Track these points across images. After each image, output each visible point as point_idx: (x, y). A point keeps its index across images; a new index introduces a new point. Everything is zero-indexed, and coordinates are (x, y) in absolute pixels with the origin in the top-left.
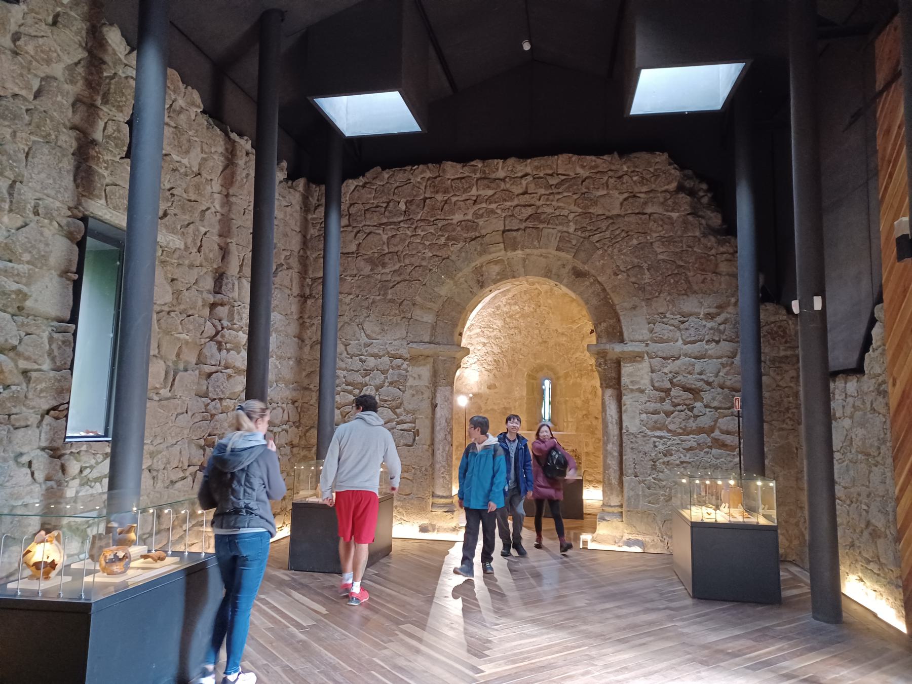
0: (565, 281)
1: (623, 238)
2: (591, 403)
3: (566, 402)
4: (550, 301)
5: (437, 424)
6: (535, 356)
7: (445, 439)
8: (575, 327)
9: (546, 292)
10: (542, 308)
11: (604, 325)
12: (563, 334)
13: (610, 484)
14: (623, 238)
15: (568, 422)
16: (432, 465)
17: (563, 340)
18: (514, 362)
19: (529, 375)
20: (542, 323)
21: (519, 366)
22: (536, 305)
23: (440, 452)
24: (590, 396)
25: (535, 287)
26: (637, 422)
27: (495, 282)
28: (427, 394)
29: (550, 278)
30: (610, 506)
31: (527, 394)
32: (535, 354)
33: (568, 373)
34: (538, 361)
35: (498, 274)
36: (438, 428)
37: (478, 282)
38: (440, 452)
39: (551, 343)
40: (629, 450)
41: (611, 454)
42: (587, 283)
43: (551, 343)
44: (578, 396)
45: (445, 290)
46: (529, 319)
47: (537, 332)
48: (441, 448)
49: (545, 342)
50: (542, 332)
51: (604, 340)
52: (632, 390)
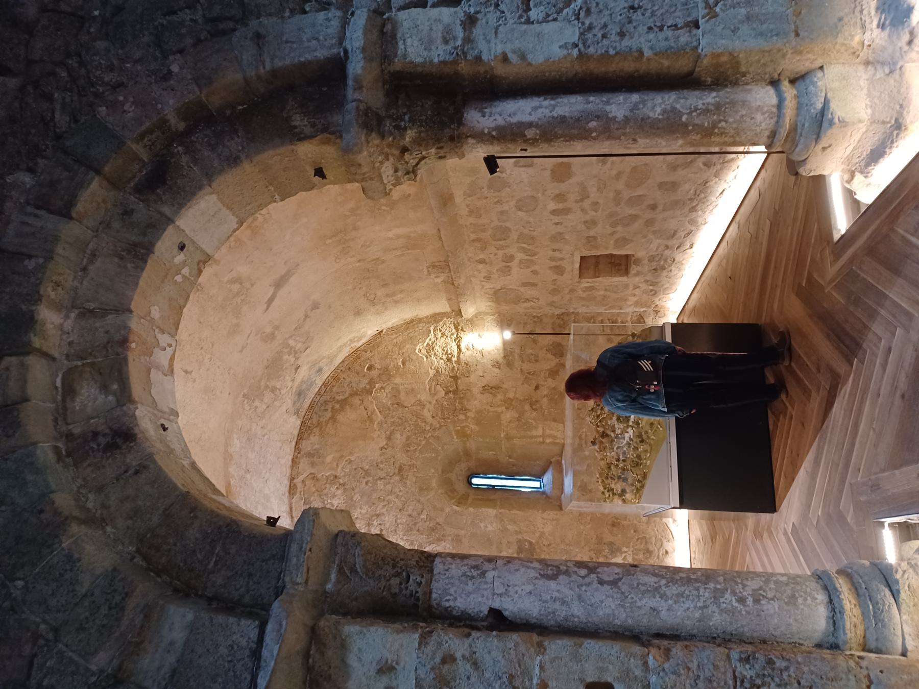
0: (166, 210)
1: (82, 64)
2: (511, 395)
3: (509, 438)
4: (329, 459)
5: (562, 613)
6: (424, 488)
7: (614, 583)
8: (379, 417)
9: (313, 464)
10: (339, 472)
11: (298, 120)
12: (389, 438)
13: (718, 106)
14: (82, 64)
15: (543, 436)
16: (724, 640)
17: (399, 439)
18: (433, 530)
19: (459, 503)
20: (367, 473)
21: (440, 520)
22: (332, 483)
23: (662, 605)
24: (500, 397)
25: (299, 485)
26: (548, 28)
27: (125, 396)
28: (453, 642)
29: (149, 249)
30: (780, 106)
31: (494, 507)
32: (421, 489)
33: (457, 432)
34: (434, 484)
35: (104, 388)
36: (577, 612)
37: (111, 447)
38: (662, 605)
39: (402, 458)
40: (626, 42)
41: (635, 107)
42: (184, 159)
43: (402, 458)
44: (498, 416)
45: (95, 553)
46: (357, 497)
47: (380, 485)
48: (649, 602)
49: (401, 469)
50: (382, 474)
51: (337, 118)
52: (468, 40)
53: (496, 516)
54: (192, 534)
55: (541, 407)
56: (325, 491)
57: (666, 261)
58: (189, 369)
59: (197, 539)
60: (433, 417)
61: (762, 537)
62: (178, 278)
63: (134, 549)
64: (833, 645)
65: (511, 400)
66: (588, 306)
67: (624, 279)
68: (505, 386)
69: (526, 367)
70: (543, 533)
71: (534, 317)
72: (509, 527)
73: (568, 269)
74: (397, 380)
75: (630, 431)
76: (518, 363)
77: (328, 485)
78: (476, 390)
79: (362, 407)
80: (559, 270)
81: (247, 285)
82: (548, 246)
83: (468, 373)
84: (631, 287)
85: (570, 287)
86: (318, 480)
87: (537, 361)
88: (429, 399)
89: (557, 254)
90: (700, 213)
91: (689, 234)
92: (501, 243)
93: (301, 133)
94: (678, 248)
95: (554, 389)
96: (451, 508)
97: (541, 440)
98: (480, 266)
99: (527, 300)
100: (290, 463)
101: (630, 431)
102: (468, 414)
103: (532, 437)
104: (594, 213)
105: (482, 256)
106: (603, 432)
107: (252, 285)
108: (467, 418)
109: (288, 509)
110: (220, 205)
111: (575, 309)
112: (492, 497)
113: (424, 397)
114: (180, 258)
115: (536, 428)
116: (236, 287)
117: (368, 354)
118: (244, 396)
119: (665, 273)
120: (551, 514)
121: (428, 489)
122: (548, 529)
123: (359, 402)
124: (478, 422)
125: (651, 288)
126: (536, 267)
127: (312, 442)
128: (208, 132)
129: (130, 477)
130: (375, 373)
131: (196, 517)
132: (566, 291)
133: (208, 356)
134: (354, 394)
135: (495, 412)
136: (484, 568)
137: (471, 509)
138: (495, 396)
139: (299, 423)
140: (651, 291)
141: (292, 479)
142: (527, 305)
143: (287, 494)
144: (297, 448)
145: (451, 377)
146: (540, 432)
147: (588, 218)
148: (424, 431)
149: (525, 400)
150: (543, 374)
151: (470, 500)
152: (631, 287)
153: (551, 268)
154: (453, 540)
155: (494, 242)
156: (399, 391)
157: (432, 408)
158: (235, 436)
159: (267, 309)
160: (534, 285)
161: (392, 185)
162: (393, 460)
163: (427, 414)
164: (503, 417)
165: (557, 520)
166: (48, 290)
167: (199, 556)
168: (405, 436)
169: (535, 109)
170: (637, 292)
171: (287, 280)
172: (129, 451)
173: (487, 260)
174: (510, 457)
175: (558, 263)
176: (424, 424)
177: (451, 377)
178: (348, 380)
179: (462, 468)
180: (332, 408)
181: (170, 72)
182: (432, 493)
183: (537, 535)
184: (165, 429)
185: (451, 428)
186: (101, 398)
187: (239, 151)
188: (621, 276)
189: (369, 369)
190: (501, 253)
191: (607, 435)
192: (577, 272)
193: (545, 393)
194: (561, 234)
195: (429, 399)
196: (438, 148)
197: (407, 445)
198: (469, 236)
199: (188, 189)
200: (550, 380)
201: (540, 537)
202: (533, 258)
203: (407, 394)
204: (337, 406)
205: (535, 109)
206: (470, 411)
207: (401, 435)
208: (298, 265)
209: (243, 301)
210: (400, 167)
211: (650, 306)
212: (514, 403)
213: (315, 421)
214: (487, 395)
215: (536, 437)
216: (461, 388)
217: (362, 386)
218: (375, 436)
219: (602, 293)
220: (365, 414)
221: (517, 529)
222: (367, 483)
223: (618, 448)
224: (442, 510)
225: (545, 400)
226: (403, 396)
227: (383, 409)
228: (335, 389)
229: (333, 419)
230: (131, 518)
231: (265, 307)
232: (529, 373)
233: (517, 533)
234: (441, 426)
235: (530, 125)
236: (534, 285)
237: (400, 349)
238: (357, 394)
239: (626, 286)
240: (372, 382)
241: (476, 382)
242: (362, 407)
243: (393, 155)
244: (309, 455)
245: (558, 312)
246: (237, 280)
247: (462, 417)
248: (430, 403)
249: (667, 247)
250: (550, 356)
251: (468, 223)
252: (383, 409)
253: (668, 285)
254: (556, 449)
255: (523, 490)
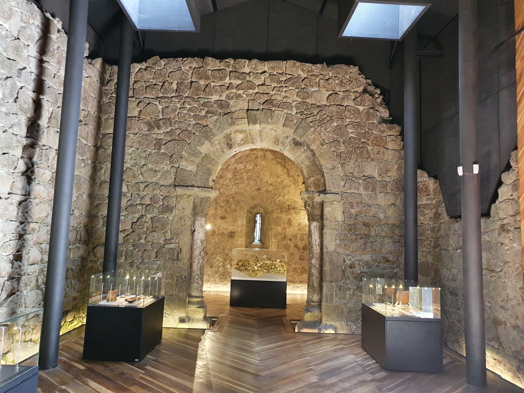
2: (287, 230)
4: (263, 163)
6: (253, 198)
12: (271, 184)
15: (272, 241)
19: (248, 211)
31: (246, 223)
32: (252, 197)
34: (254, 202)
35: (242, 140)
38: (196, 263)
39: (264, 190)
42: (302, 150)
43: (264, 190)
44: (280, 225)
48: (196, 261)
50: (258, 182)
54: (210, 166)
64: (190, 296)
68: (291, 228)
76: (300, 233)
78: (289, 216)
83: (296, 213)
87: (301, 240)
96: (246, 208)
112: (251, 223)
115: (275, 239)
121: (253, 200)
127: (270, 156)
130: (296, 177)
146: (273, 240)
148: (273, 197)
166: (263, 125)
169: (315, 240)
178: (293, 167)
181: (324, 145)
182: (251, 201)
186: (240, 139)
189: (298, 175)
197: (268, 191)
200: (293, 245)
205: (315, 240)
213: (277, 156)
224: (245, 205)
225: (285, 243)
227: (282, 182)
229: (278, 163)
233: (238, 231)
235: (311, 239)
240: (292, 176)
244: (265, 155)
247: (279, 211)
250: (303, 245)
252: (282, 182)
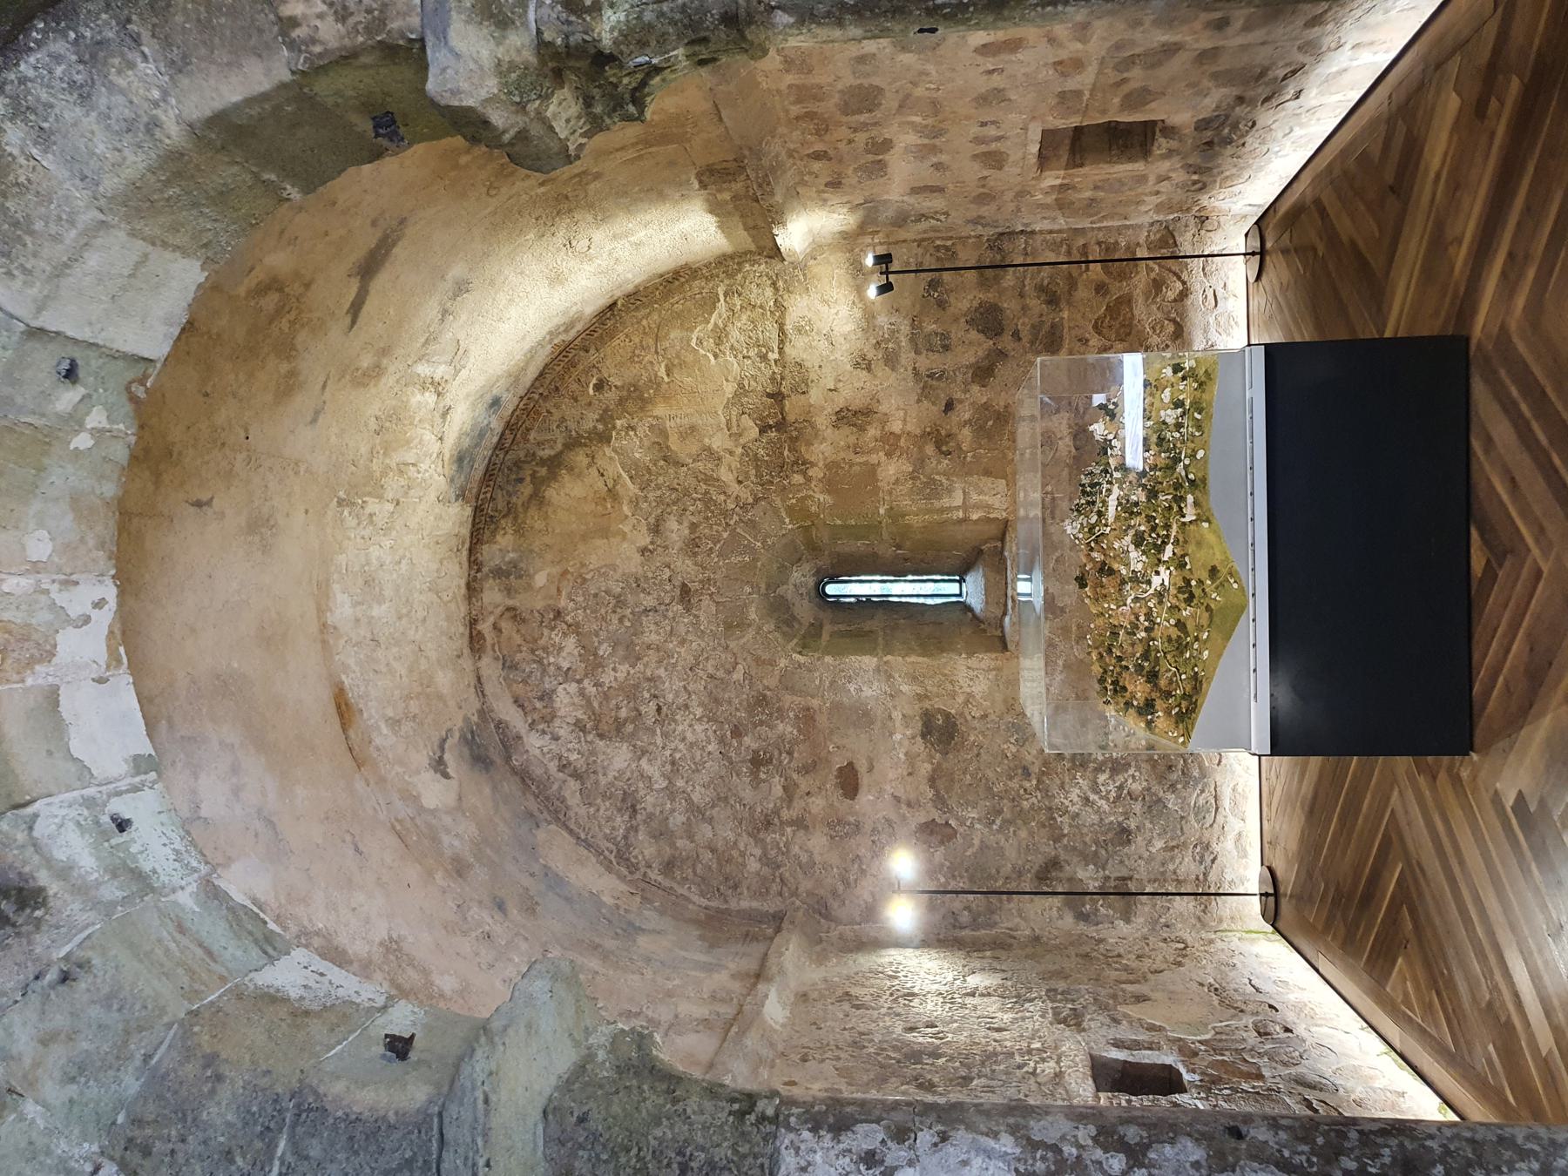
4: (540, 579)
6: (733, 624)
8: (630, 488)
9: (509, 591)
12: (656, 529)
15: (965, 507)
17: (676, 530)
19: (804, 647)
20: (620, 602)
31: (872, 652)
32: (729, 627)
39: (686, 568)
43: (686, 568)
44: (872, 471)
49: (685, 591)
50: (649, 601)
53: (878, 670)
55: (959, 447)
56: (542, 642)
57: (1235, 127)
58: (204, 497)
59: (229, 1124)
60: (740, 482)
61: (1434, 778)
62: (83, 441)
63: (95, 1148)
65: (898, 437)
66: (1054, 219)
67: (1139, 166)
68: (883, 408)
69: (925, 362)
70: (970, 695)
71: (938, 248)
72: (905, 688)
73: (1015, 155)
74: (660, 410)
75: (1165, 575)
76: (907, 357)
77: (546, 631)
78: (822, 421)
79: (593, 471)
80: (995, 160)
81: (296, 288)
82: (968, 118)
84: (1152, 179)
85: (1018, 188)
86: (524, 620)
87: (946, 348)
88: (729, 444)
89: (992, 131)
90: (1329, 27)
91: (1294, 72)
92: (864, 118)
93: (314, 41)
94: (1267, 100)
95: (986, 406)
96: (789, 658)
97: (961, 514)
98: (817, 166)
99: (922, 217)
100: (463, 590)
101: (1165, 575)
102: (810, 473)
103: (942, 510)
104: (1079, 46)
105: (819, 147)
106: (1104, 563)
107: (307, 286)
108: (809, 479)
109: (473, 681)
110: (140, 244)
111: (1026, 225)
112: (868, 626)
113: (718, 442)
114: (68, 398)
115: (950, 491)
116: (270, 301)
117: (593, 357)
118: (340, 503)
119: (1229, 150)
120: (985, 660)
121: (743, 625)
122: (980, 687)
123: (586, 461)
124: (830, 485)
125: (1195, 177)
126: (944, 158)
128: (59, 46)
129: (52, 986)
130: (611, 396)
131: (219, 1078)
132: (1009, 195)
133: (241, 457)
134: (573, 443)
135: (866, 463)
136: (889, 1161)
137: (828, 659)
138: (862, 429)
139: (469, 511)
140: (1195, 183)
141: (473, 623)
142: (924, 225)
143: (466, 651)
144: (474, 563)
145: (769, 395)
147: (1064, 55)
148: (725, 514)
149: (925, 435)
150: (960, 377)
151: (825, 636)
152: (1152, 179)
153: (975, 157)
154: (797, 717)
155: (844, 119)
156: (663, 433)
157: (736, 465)
158: (336, 587)
159: (354, 322)
160: (939, 190)
161: (583, 135)
162: (667, 573)
163: (726, 475)
164: (881, 474)
165: (998, 669)
167: (239, 1161)
168: (686, 524)
170: (1165, 187)
171: (388, 253)
172: (38, 928)
173: (831, 153)
174: (899, 547)
175: (993, 146)
176: (722, 497)
177: (769, 395)
179: (801, 576)
180: (533, 476)
182: (751, 632)
183: (960, 699)
184: (122, 825)
185: (778, 502)
187: (156, 104)
188: (1131, 160)
189: (599, 387)
190: (861, 138)
191: (1111, 572)
192: (1033, 160)
193: (967, 416)
194: (999, 91)
195: (729, 444)
196: (692, 43)
197: (692, 546)
198: (787, 111)
199: (39, 225)
200: (975, 388)
201: (967, 702)
202: (937, 142)
203: (683, 436)
204: (543, 471)
206: (813, 464)
207: (680, 523)
208: (403, 221)
209: (292, 323)
210: (596, 92)
211: (1188, 210)
212: (902, 443)
214: (846, 430)
215: (950, 509)
216: (791, 418)
217: (588, 425)
218: (626, 529)
219: (1088, 194)
220: (600, 484)
221: (919, 690)
222: (621, 620)
223: (1136, 599)
224: (772, 663)
225: (966, 431)
226: (674, 443)
228: (532, 436)
229: (537, 498)
230: (73, 1080)
231: (348, 320)
232: (931, 376)
234: (757, 500)
236: (939, 190)
237: (657, 339)
238: (581, 445)
239: (1142, 179)
240: (606, 417)
241: (820, 400)
242: (593, 471)
243: (575, 71)
244: (498, 573)
245: (989, 232)
246: (274, 284)
247: (798, 479)
248: (731, 453)
249: (1240, 100)
250: (974, 335)
251: (783, 87)
252: (639, 473)
253: (1234, 171)
254: (993, 530)
255: (930, 601)
